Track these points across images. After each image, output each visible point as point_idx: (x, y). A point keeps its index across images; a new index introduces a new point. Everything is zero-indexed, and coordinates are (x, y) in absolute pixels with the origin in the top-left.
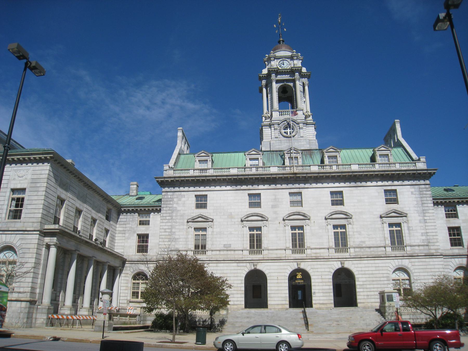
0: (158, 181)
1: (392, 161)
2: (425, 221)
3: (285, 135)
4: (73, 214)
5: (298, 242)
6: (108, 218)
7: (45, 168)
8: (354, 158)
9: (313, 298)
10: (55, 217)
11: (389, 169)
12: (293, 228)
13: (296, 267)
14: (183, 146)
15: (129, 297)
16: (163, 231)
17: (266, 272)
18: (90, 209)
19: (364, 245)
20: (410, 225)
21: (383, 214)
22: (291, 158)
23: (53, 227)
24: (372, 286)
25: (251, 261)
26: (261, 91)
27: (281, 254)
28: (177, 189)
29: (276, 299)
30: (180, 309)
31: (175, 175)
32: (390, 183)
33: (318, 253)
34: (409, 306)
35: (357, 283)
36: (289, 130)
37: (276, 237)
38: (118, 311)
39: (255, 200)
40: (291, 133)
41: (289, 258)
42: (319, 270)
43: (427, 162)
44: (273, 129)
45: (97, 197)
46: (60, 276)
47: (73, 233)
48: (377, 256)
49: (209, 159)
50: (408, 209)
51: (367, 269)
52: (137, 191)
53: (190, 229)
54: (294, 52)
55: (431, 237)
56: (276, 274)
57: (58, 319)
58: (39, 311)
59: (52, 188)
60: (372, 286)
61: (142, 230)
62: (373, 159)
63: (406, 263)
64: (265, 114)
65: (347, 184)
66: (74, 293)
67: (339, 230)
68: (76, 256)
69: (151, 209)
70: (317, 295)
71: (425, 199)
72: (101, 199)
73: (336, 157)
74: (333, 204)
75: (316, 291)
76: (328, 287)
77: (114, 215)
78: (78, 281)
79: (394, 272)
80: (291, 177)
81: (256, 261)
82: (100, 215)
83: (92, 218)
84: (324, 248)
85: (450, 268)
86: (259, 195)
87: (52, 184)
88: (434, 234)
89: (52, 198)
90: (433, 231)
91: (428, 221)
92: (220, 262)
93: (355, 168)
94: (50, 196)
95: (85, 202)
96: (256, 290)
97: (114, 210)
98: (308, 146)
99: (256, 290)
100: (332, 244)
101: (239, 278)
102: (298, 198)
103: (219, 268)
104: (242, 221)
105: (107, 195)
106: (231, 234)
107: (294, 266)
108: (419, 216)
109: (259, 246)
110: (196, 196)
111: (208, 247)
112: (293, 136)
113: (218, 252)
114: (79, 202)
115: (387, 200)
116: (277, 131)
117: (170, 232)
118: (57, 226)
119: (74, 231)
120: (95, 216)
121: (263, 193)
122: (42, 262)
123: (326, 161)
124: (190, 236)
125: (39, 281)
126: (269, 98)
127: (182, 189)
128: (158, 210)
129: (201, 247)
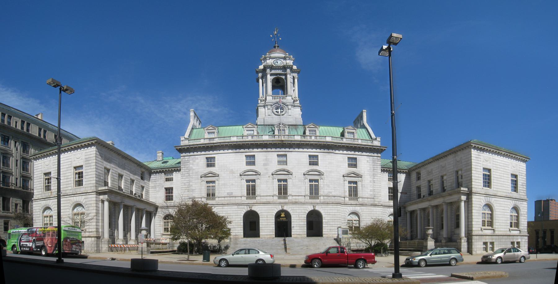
0: (177, 149)
1: (356, 137)
2: (374, 182)
3: (276, 113)
4: (117, 178)
5: (283, 191)
6: (142, 178)
7: (92, 150)
8: (329, 133)
9: (292, 231)
10: (105, 181)
11: (353, 143)
12: (279, 180)
13: (281, 209)
14: (195, 123)
15: (162, 231)
17: (259, 212)
18: (128, 173)
19: (331, 195)
20: (363, 183)
22: (279, 130)
23: (104, 188)
24: (333, 223)
25: (247, 204)
26: (258, 81)
27: (270, 199)
28: (192, 154)
29: (265, 231)
30: (197, 239)
31: (190, 144)
32: (353, 152)
34: (355, 238)
35: (324, 221)
36: (279, 110)
37: (267, 187)
38: (154, 241)
39: (251, 160)
40: (279, 112)
43: (381, 141)
44: (266, 109)
45: (133, 164)
46: (113, 220)
47: (118, 191)
49: (216, 131)
51: (331, 211)
52: (163, 157)
56: (266, 214)
57: (115, 247)
58: (103, 243)
59: (100, 163)
60: (333, 223)
61: (168, 185)
62: (342, 135)
63: (358, 209)
64: (260, 98)
65: (322, 150)
66: (124, 230)
68: (122, 206)
69: (173, 169)
70: (295, 228)
72: (136, 165)
73: (315, 131)
74: (310, 164)
75: (295, 226)
76: (303, 223)
77: (146, 175)
78: (126, 222)
79: (349, 215)
82: (136, 177)
83: (131, 179)
86: (254, 156)
87: (100, 160)
89: (101, 169)
93: (328, 139)
94: (99, 168)
95: (124, 169)
96: (251, 224)
97: (146, 173)
99: (251, 224)
100: (308, 193)
101: (239, 217)
102: (284, 159)
103: (224, 210)
105: (140, 162)
106: (232, 185)
107: (280, 208)
109: (254, 193)
111: (216, 195)
112: (283, 115)
113: (223, 199)
114: (120, 169)
115: (349, 165)
116: (270, 111)
117: (188, 186)
118: (106, 188)
119: (119, 190)
120: (132, 178)
122: (100, 212)
123: (307, 133)
125: (100, 224)
126: (264, 86)
127: (195, 153)
129: (211, 195)
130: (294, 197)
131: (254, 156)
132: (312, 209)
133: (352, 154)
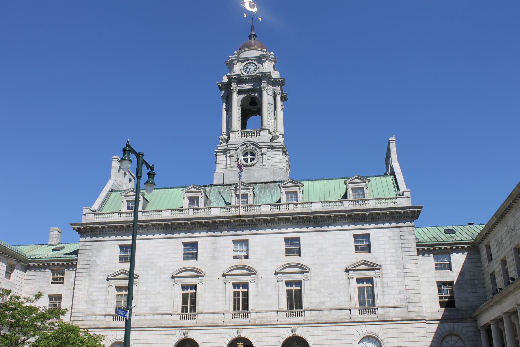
5: (241, 302)
8: (321, 193)
13: (236, 336)
16: (83, 290)
20: (385, 280)
21: (349, 267)
33: (264, 318)
36: (249, 157)
39: (191, 251)
41: (228, 324)
42: (264, 339)
44: (228, 155)
48: (339, 321)
50: (383, 259)
53: (110, 288)
54: (235, 54)
55: (412, 296)
61: (56, 290)
63: (375, 330)
67: (365, 285)
71: (407, 245)
79: (361, 341)
80: (234, 221)
81: (188, 328)
84: (272, 311)
85: (354, 338)
88: (416, 291)
90: (415, 287)
91: (408, 275)
92: (144, 329)
98: (272, 177)
104: (173, 277)
108: (397, 268)
110: (354, 235)
112: (254, 165)
113: (142, 317)
116: (234, 159)
121: (373, 233)
124: (110, 297)
128: (74, 266)
130: (259, 315)
131: (196, 244)
132: (291, 334)
133: (361, 229)
